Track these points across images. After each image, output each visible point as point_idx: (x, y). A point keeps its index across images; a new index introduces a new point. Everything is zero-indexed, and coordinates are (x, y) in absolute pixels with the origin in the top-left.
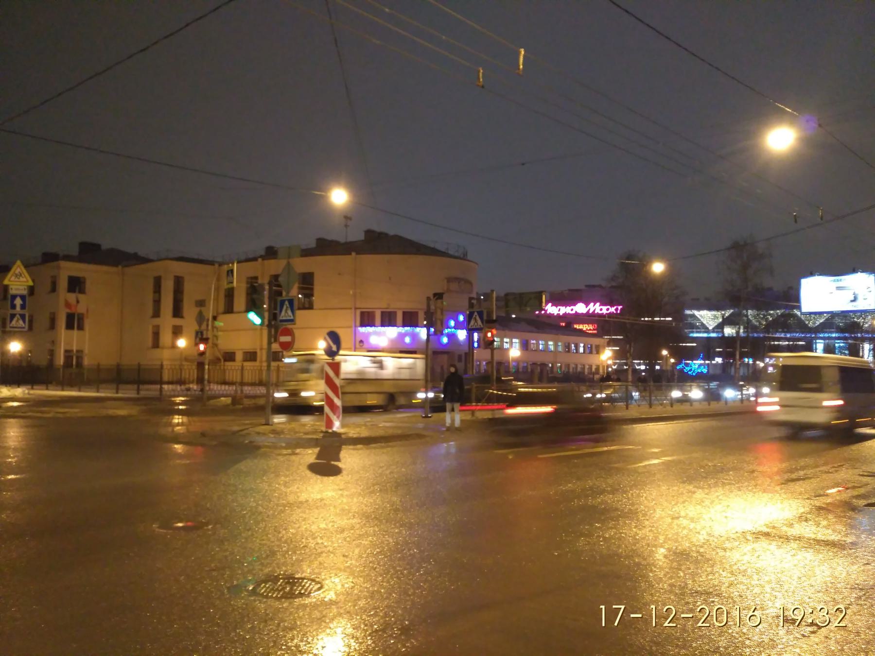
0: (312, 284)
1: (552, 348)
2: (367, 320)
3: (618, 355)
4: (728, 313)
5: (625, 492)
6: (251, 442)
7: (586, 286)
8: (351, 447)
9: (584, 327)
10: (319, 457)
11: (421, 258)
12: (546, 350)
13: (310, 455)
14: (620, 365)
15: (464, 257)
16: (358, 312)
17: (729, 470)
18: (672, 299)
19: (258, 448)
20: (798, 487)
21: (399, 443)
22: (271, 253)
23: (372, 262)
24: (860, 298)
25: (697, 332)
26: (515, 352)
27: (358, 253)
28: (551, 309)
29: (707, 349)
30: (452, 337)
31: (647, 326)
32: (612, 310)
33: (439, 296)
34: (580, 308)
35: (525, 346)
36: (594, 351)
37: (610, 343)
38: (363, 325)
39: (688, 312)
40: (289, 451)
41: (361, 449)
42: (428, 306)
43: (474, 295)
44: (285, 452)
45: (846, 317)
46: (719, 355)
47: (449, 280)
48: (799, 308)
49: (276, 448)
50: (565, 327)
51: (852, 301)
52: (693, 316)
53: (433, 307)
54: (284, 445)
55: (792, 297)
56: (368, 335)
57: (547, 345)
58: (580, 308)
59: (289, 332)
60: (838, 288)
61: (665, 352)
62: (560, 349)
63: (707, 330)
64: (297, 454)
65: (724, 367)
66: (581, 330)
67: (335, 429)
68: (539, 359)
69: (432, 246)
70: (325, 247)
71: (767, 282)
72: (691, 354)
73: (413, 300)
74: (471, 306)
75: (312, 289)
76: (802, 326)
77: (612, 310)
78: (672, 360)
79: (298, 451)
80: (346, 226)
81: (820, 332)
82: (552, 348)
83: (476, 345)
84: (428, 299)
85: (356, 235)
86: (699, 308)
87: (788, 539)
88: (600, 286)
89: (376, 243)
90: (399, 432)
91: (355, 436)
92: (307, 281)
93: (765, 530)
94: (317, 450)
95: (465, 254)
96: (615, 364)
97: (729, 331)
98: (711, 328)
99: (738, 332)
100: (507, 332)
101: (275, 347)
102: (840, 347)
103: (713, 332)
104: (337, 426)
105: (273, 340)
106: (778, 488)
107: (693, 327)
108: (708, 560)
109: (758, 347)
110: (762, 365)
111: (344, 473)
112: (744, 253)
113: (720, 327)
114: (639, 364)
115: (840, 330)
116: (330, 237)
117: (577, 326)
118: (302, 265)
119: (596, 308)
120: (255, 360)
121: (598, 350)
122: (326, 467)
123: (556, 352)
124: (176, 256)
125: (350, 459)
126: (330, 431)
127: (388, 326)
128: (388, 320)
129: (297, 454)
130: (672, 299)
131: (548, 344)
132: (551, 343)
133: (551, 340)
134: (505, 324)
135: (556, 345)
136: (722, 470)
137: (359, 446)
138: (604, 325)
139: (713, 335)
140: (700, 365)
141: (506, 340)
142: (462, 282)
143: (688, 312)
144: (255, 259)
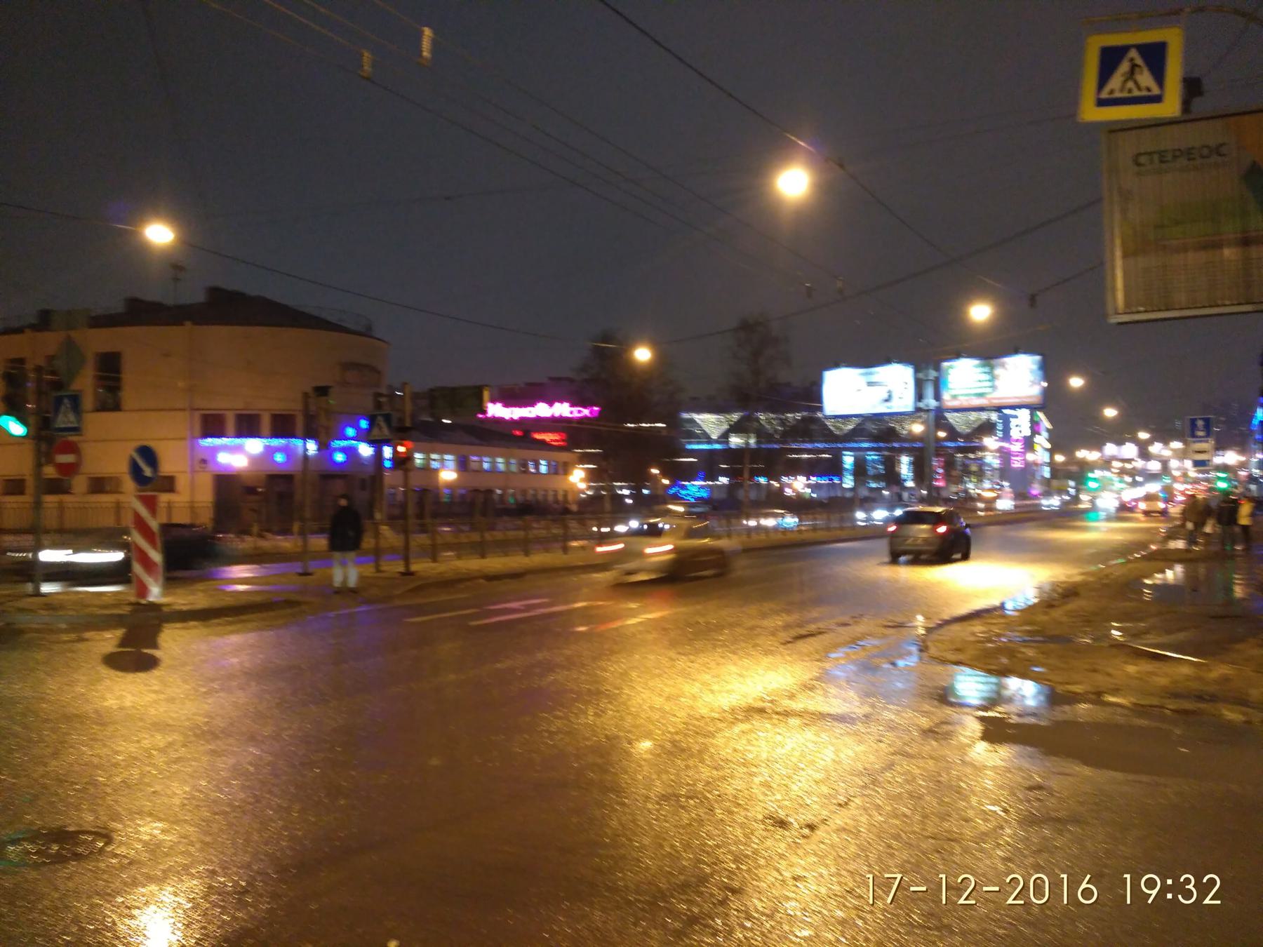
0: (118, 371)
1: (501, 467)
2: (213, 426)
3: (592, 476)
4: (735, 417)
5: (583, 665)
6: (8, 624)
7: (551, 379)
8: (178, 625)
9: (548, 437)
10: (124, 642)
11: (261, 333)
12: (494, 471)
13: (109, 640)
14: (597, 489)
15: (367, 333)
16: (197, 415)
17: (723, 627)
18: (664, 397)
19: (21, 632)
20: (802, 646)
21: (260, 615)
22: (44, 321)
23: (219, 337)
24: (895, 396)
25: (699, 443)
26: (448, 475)
27: (196, 323)
28: (496, 410)
29: (708, 465)
30: (351, 452)
31: (631, 436)
32: (586, 412)
33: (322, 391)
34: (542, 410)
35: (463, 465)
36: (561, 471)
37: (584, 459)
38: (206, 435)
39: (686, 416)
40: (73, 636)
41: (195, 627)
42: (306, 405)
43: (384, 391)
44: (65, 637)
45: (880, 421)
46: (724, 473)
47: (347, 366)
48: (821, 409)
49: (51, 631)
50: (520, 436)
51: (886, 401)
52: (692, 421)
53: (313, 408)
54: (64, 626)
55: (813, 395)
56: (215, 450)
57: (494, 463)
58: (542, 410)
59: (71, 448)
60: (870, 384)
61: (655, 471)
62: (514, 468)
63: (709, 441)
64: (87, 640)
65: (730, 488)
66: (543, 442)
67: (151, 599)
68: (482, 483)
69: (316, 313)
70: (141, 312)
71: (784, 375)
72: (688, 473)
73: (284, 397)
74: (379, 406)
75: (118, 380)
76: (829, 436)
77: (586, 412)
78: (666, 482)
79: (88, 635)
80: (176, 279)
81: (849, 441)
82: (501, 467)
83: (388, 464)
84: (306, 395)
85: (193, 294)
86: (699, 411)
87: (787, 714)
88: (571, 380)
89: (225, 307)
90: (258, 599)
91: (184, 608)
92: (110, 367)
93: (760, 704)
94: (120, 633)
95: (369, 328)
96: (589, 488)
97: (736, 441)
98: (714, 437)
99: (747, 444)
100: (438, 445)
101: (50, 471)
102: (873, 461)
103: (717, 442)
104: (155, 593)
105: (43, 460)
106: (781, 648)
107: (691, 436)
108: (683, 750)
109: (774, 461)
110: (776, 484)
111: (163, 665)
112: (755, 337)
113: (725, 437)
114: (621, 488)
115: (875, 438)
116: (149, 297)
117: (538, 436)
118: (98, 341)
119: (563, 409)
120: (22, 493)
121: (566, 469)
122: (135, 656)
123: (507, 474)
124: (323, 335)
125: (173, 642)
126: (143, 602)
127: (246, 437)
128: (248, 428)
129: (87, 640)
130: (664, 397)
131: (494, 462)
132: (500, 460)
133: (501, 456)
134: (432, 435)
135: (508, 463)
136: (719, 628)
137: (192, 623)
138: (572, 432)
139: (717, 446)
140: (702, 487)
141: (434, 456)
142: (364, 371)
143: (686, 416)
144: (19, 331)
